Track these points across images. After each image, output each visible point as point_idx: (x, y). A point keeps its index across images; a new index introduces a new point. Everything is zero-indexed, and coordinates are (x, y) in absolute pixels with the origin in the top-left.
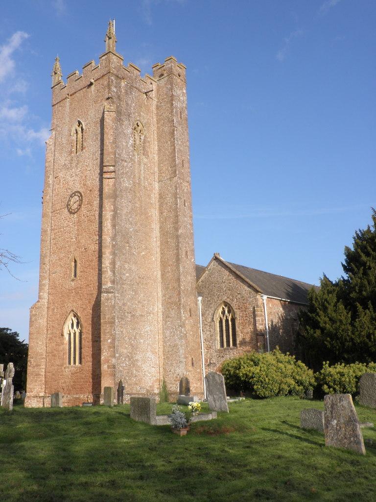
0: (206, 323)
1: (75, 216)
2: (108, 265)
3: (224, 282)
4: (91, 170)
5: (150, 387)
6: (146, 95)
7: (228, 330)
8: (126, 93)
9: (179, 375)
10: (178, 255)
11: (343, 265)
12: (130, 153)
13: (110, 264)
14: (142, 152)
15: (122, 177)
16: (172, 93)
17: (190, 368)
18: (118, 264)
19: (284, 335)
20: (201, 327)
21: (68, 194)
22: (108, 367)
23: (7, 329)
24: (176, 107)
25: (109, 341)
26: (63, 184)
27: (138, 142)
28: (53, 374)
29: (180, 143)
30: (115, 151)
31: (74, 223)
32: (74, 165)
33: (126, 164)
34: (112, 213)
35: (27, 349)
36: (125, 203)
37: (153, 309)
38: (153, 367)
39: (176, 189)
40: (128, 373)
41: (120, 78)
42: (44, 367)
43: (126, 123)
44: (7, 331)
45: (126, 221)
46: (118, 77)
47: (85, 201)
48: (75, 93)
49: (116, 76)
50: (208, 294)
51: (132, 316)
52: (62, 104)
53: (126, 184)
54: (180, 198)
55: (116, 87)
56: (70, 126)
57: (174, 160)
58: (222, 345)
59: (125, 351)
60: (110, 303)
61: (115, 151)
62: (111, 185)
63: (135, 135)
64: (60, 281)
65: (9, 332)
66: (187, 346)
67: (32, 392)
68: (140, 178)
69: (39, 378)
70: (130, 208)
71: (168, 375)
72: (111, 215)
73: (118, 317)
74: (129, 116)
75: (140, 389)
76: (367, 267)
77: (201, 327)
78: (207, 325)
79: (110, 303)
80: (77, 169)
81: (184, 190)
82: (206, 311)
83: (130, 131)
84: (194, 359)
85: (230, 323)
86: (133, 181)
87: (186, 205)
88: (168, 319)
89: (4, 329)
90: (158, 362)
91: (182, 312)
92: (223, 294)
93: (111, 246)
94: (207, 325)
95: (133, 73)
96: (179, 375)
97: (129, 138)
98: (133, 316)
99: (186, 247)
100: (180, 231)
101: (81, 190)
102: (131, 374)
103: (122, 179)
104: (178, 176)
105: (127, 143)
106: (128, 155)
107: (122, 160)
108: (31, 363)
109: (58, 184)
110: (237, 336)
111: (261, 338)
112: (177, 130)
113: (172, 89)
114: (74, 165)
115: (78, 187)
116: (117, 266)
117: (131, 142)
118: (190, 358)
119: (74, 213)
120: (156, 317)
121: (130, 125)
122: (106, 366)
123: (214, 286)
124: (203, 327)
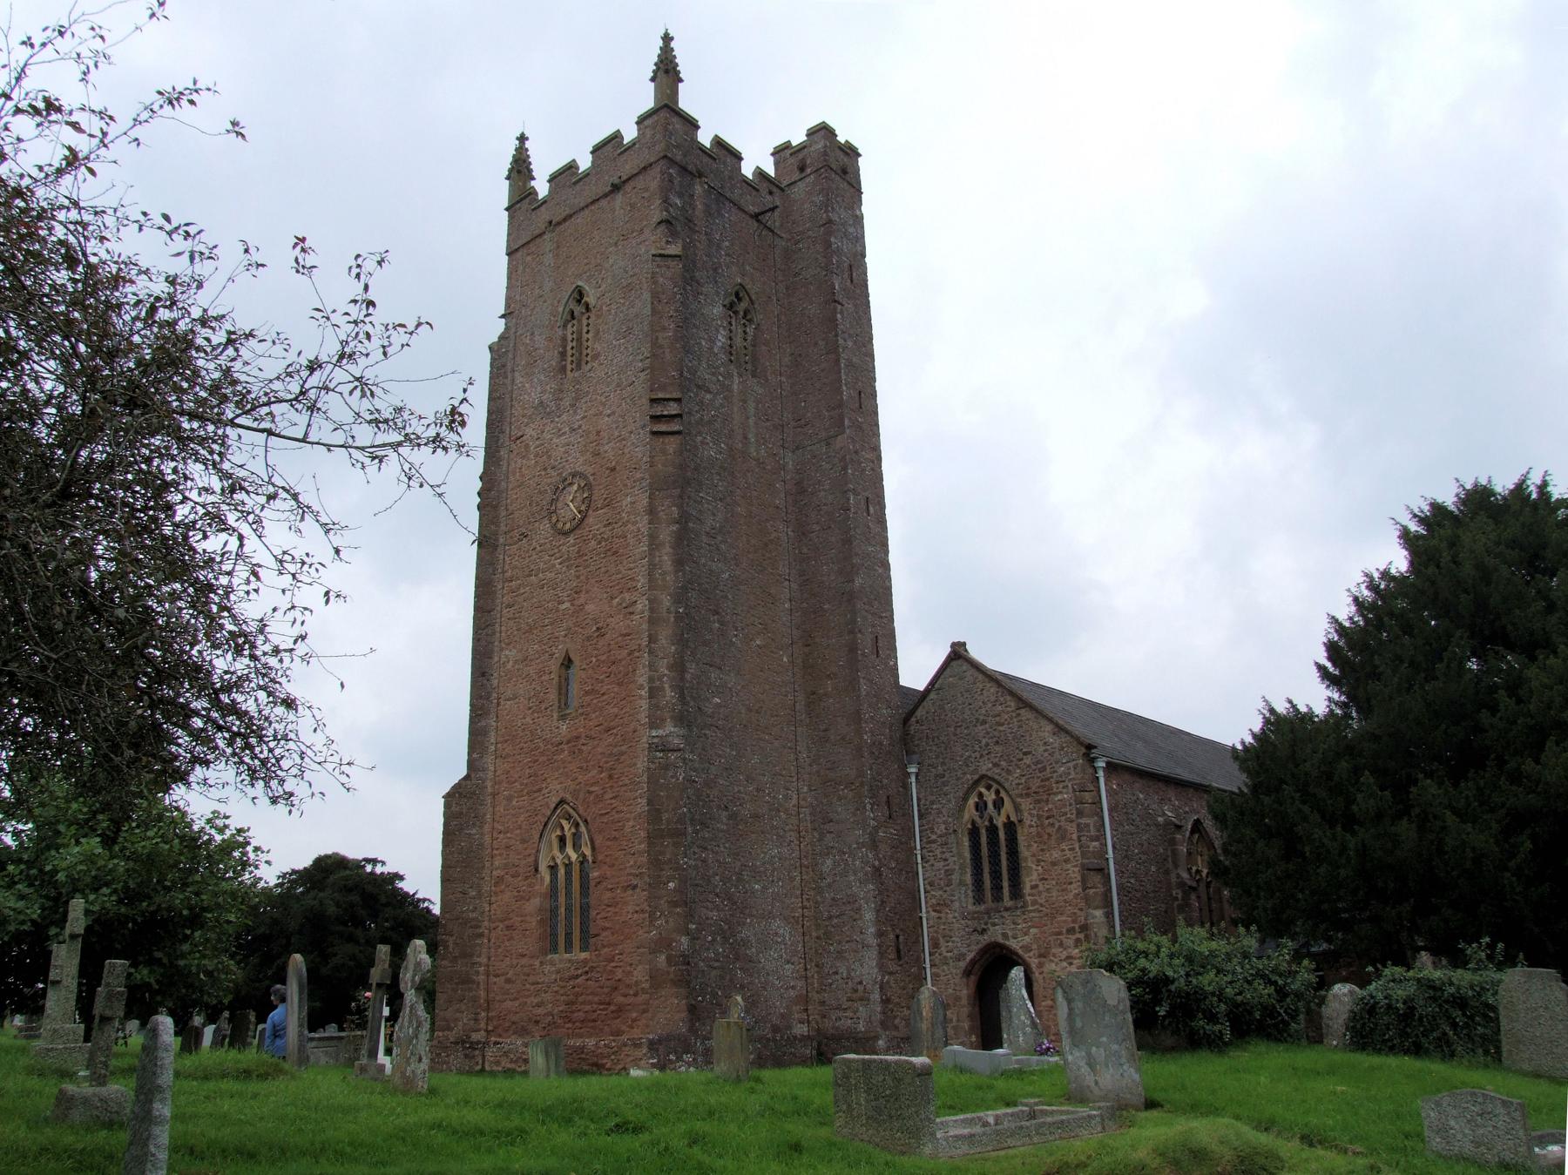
0: (934, 837)
1: (571, 539)
2: (666, 672)
3: (984, 722)
4: (614, 413)
5: (782, 1015)
6: (758, 221)
7: (994, 856)
8: (708, 212)
9: (861, 983)
10: (853, 649)
11: (1321, 668)
12: (718, 367)
13: (670, 667)
14: (749, 367)
15: (700, 433)
16: (828, 216)
17: (893, 967)
18: (692, 668)
19: (1372, 830)
20: (918, 847)
21: (549, 481)
22: (669, 959)
23: (374, 861)
24: (839, 252)
25: (671, 885)
26: (536, 456)
27: (738, 341)
28: (508, 981)
29: (850, 344)
30: (682, 360)
31: (569, 559)
32: (566, 403)
33: (708, 396)
34: (675, 528)
35: (1436, 517)
36: (709, 502)
37: (786, 797)
38: (788, 962)
39: (845, 468)
40: (722, 977)
41: (691, 173)
42: (484, 960)
43: (708, 289)
44: (374, 865)
45: (710, 551)
46: (685, 169)
47: (599, 494)
48: (570, 216)
49: (681, 167)
50: (937, 757)
51: (730, 817)
52: (532, 248)
53: (711, 452)
54: (856, 493)
55: (680, 195)
56: (556, 302)
57: (839, 391)
58: (979, 899)
59: (714, 914)
60: (672, 777)
61: (682, 360)
62: (671, 451)
63: (730, 324)
64: (528, 720)
65: (379, 869)
66: (883, 902)
67: (449, 1029)
68: (746, 438)
69: (470, 990)
70: (720, 516)
71: (831, 984)
72: (673, 532)
73: (692, 820)
74: (715, 270)
75: (756, 1022)
76: (226, 1014)
77: (918, 847)
78: (934, 842)
79: (672, 777)
80: (575, 412)
81: (864, 470)
82: (932, 803)
83: (718, 310)
84: (901, 938)
85: (984, 839)
86: (727, 445)
87: (871, 509)
88: (827, 827)
89: (368, 861)
90: (800, 947)
91: (868, 807)
92: (982, 756)
93: (672, 619)
94: (934, 842)
95: (724, 163)
96: (861, 983)
97: (718, 331)
98: (733, 816)
99: (873, 626)
100: (858, 582)
101: (589, 470)
102: (731, 980)
103: (699, 438)
104: (848, 431)
105: (712, 341)
106: (713, 374)
107: (698, 387)
108: (446, 947)
109: (523, 457)
110: (1023, 872)
111: (1096, 879)
112: (842, 313)
113: (827, 206)
114: (566, 403)
115: (578, 462)
116: (688, 676)
117: (722, 339)
118: (892, 936)
119: (566, 534)
120: (794, 821)
121: (718, 294)
122: (663, 957)
123: (955, 735)
124: (922, 849)
